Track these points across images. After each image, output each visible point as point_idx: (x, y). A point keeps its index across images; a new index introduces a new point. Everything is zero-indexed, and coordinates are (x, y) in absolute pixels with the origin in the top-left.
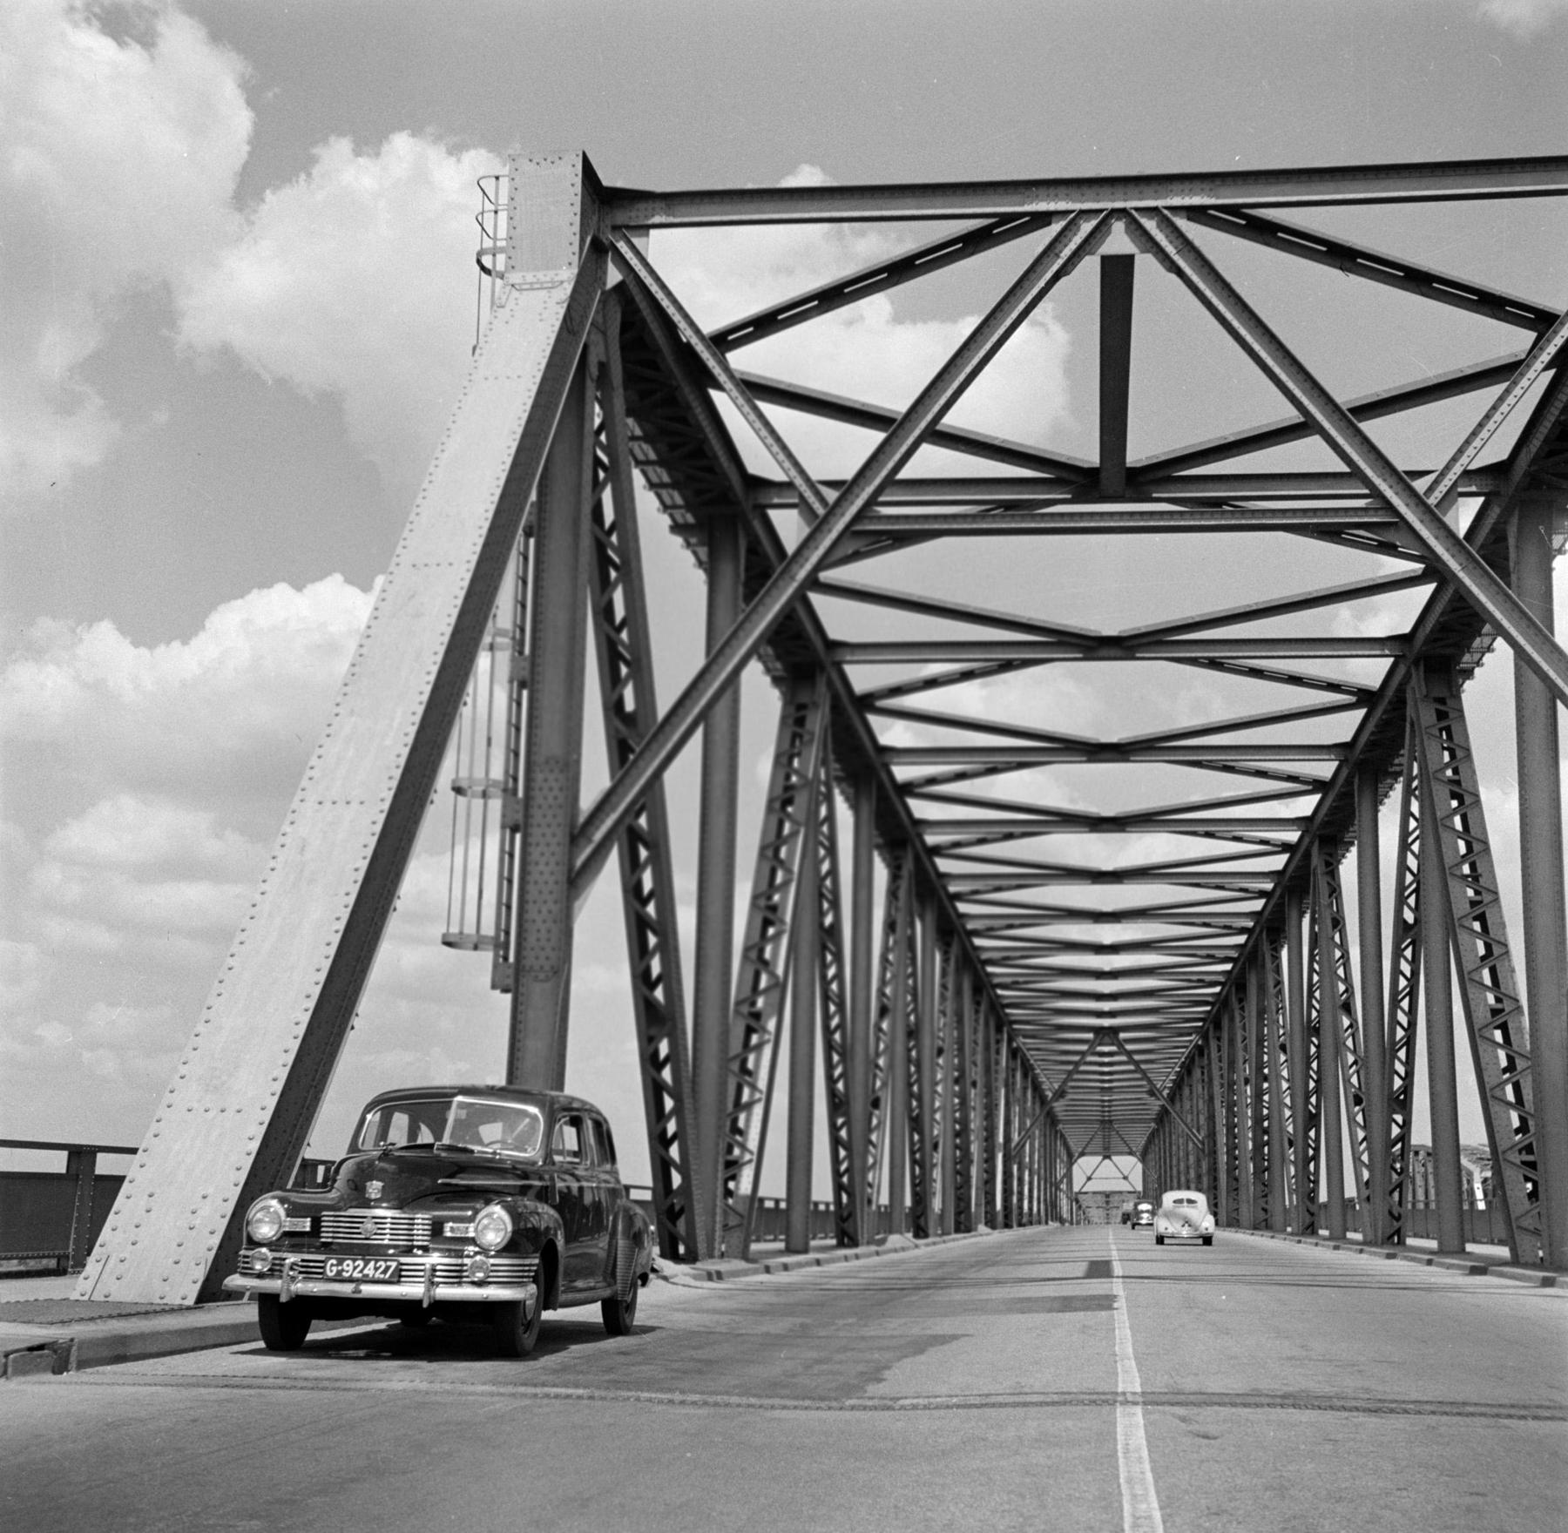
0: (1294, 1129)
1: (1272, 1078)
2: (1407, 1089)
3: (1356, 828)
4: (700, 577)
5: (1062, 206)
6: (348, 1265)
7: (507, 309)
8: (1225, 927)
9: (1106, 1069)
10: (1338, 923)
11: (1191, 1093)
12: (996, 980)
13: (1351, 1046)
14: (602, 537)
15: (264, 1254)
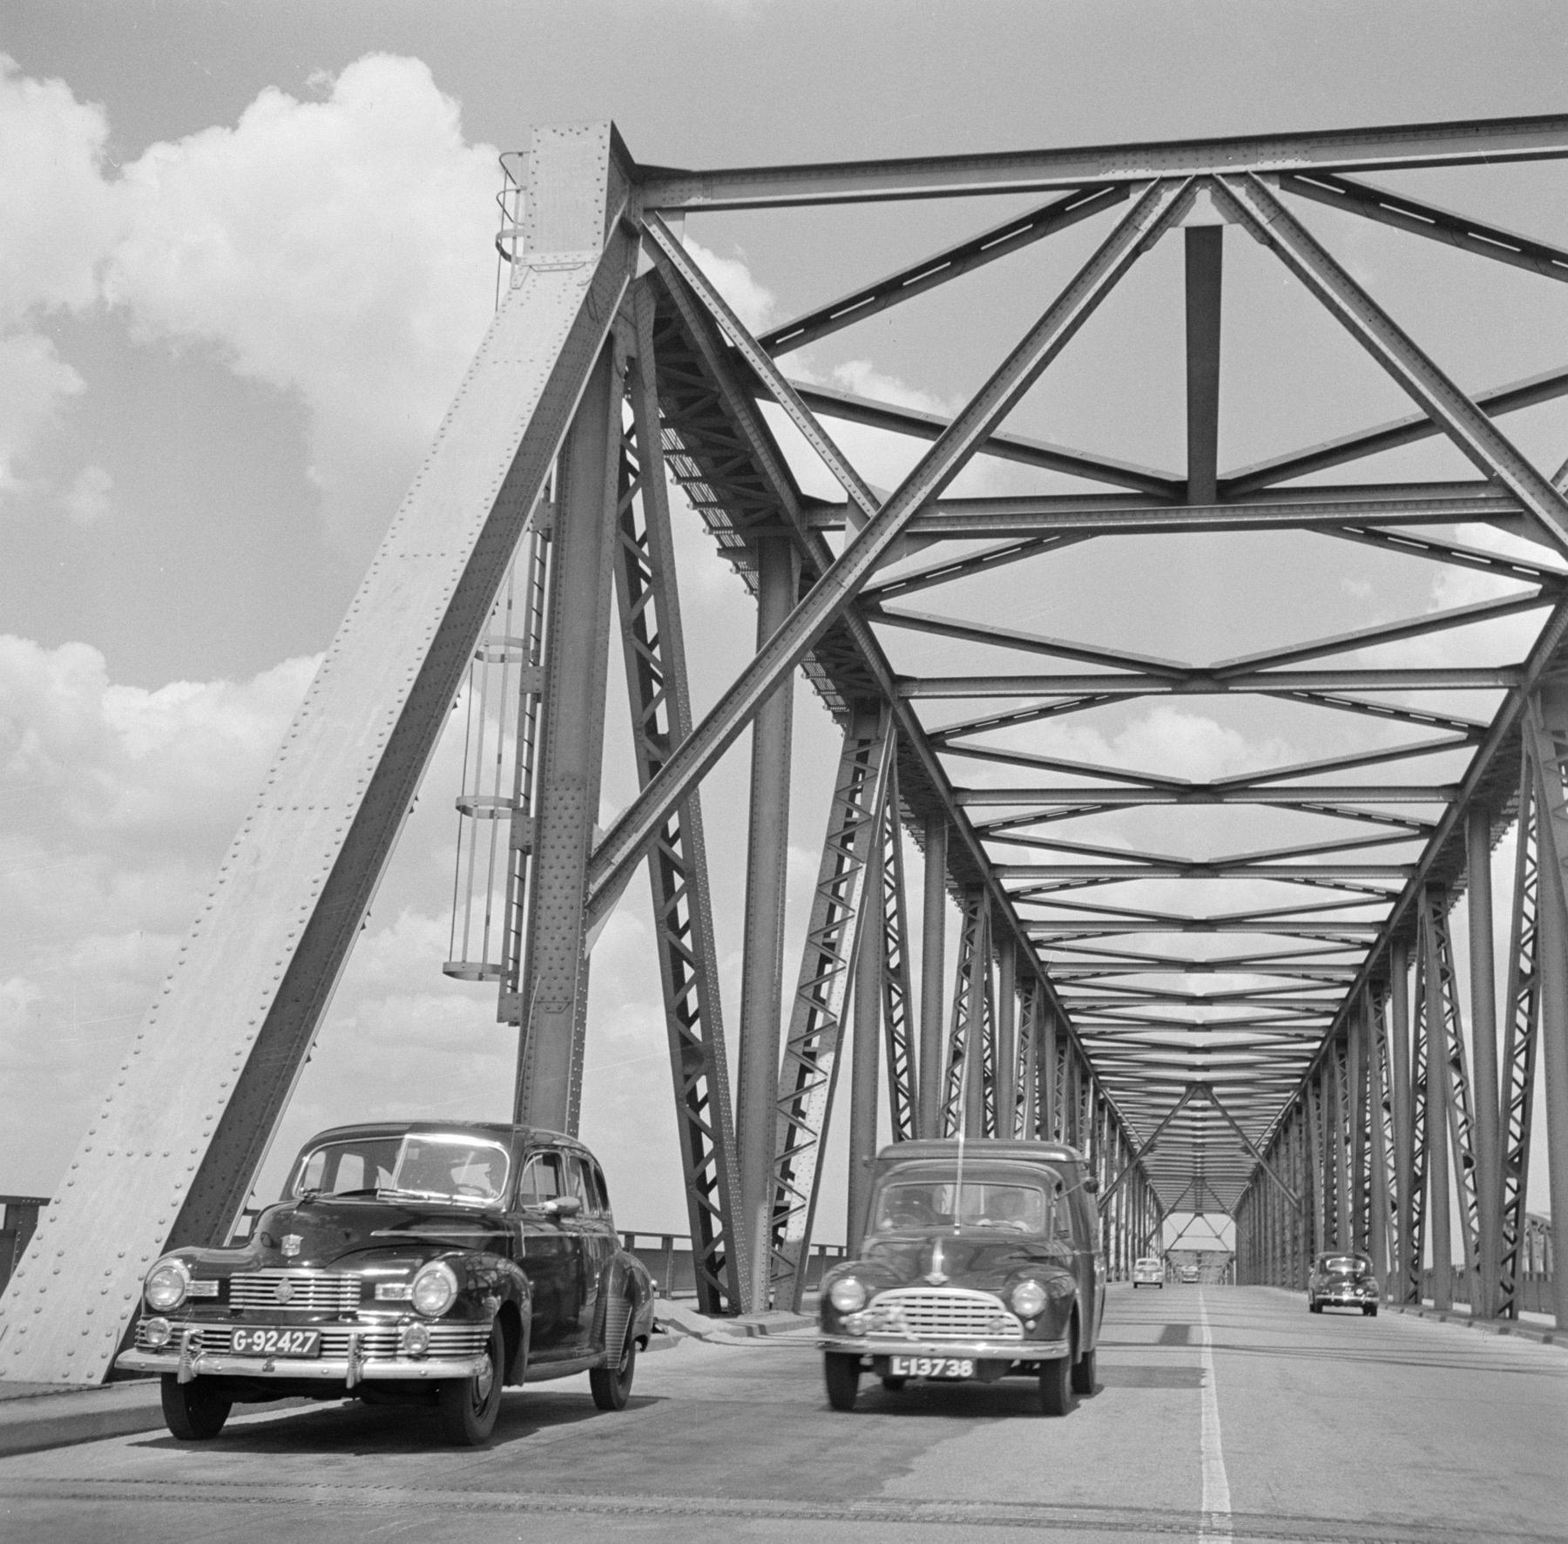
0: (1398, 1191)
1: (1375, 1137)
2: (1522, 1152)
3: (1464, 875)
4: (753, 603)
5: (1141, 173)
6: (259, 1337)
7: (524, 290)
8: (1326, 980)
9: (1199, 1124)
10: (1447, 974)
11: (1288, 1151)
12: (1081, 1031)
13: (1461, 1105)
14: (633, 548)
15: (163, 1325)
